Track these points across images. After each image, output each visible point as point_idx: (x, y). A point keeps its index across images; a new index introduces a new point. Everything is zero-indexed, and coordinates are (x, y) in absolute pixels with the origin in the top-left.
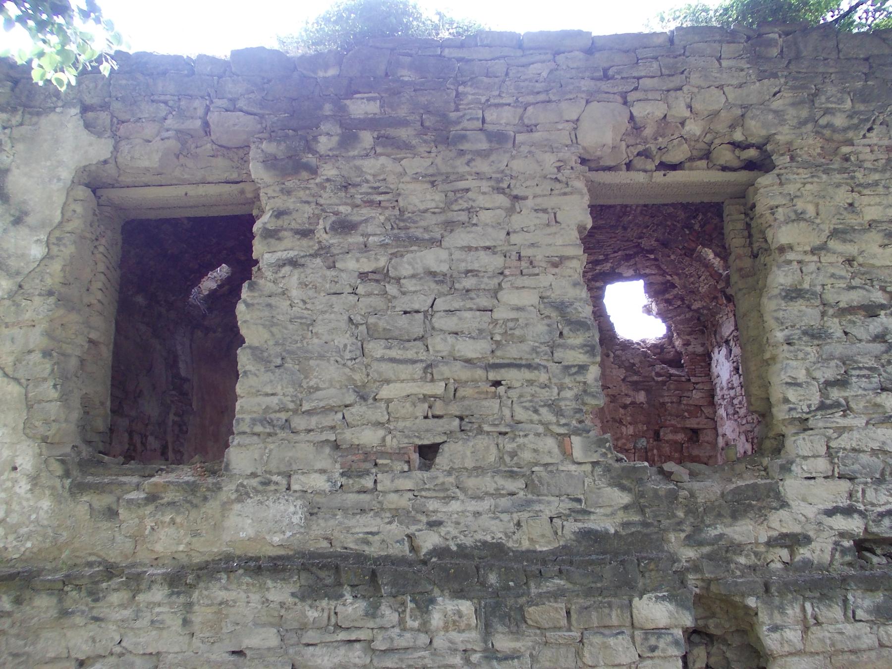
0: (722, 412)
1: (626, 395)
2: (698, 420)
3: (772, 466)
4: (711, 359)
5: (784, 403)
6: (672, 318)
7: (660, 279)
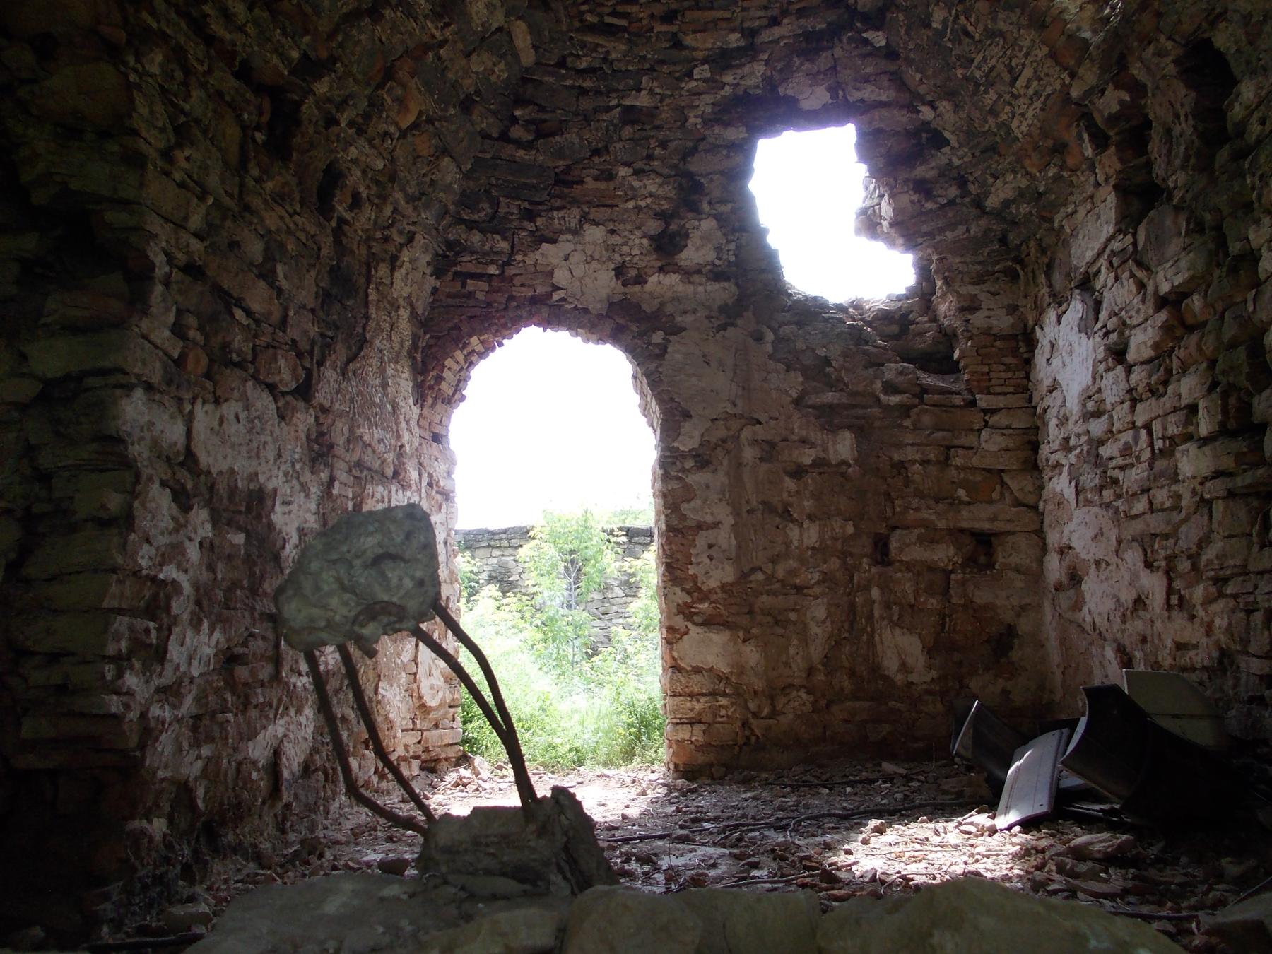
0: (1061, 485)
1: (803, 441)
2: (991, 509)
4: (1032, 344)
6: (931, 235)
7: (901, 118)
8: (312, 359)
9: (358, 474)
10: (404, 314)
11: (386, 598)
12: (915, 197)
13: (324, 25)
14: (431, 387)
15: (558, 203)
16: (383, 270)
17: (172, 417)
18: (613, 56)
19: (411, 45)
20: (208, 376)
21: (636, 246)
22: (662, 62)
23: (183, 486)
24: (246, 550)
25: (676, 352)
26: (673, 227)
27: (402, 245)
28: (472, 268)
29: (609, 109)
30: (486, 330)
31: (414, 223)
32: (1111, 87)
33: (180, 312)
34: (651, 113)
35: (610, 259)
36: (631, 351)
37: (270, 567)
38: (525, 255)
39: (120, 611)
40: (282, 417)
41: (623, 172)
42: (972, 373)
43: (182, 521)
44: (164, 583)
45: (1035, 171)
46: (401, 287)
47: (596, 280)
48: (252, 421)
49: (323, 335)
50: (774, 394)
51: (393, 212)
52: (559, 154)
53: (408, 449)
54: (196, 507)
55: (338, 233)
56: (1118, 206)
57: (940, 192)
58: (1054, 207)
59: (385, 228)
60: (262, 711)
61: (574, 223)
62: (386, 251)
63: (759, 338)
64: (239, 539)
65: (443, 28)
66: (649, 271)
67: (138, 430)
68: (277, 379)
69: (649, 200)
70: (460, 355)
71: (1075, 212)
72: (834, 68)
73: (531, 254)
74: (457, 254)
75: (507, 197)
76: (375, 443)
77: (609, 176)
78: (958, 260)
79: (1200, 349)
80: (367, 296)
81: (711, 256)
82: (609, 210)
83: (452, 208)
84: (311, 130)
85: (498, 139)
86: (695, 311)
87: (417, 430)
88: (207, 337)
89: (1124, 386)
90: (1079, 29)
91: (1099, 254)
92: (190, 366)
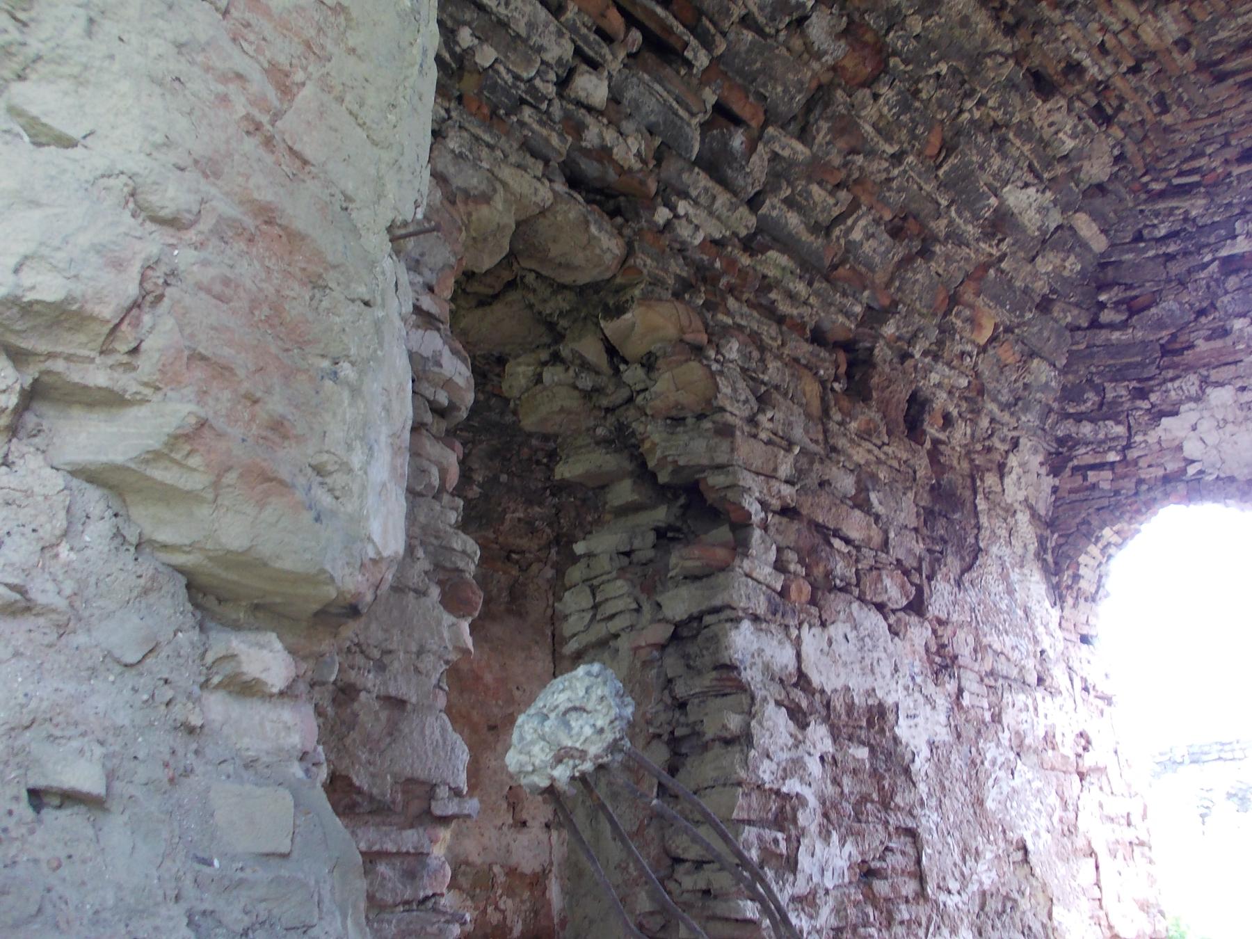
8: (921, 575)
9: (992, 683)
10: (1023, 518)
11: (570, 744)
13: (880, 277)
14: (1069, 587)
15: (1171, 373)
16: (991, 479)
17: (780, 642)
19: (970, 269)
20: (813, 601)
23: (799, 706)
24: (871, 764)
27: (1007, 452)
28: (1090, 459)
29: (1205, 266)
30: (1119, 519)
31: (1015, 428)
33: (779, 550)
37: (901, 780)
38: (1145, 434)
39: (750, 822)
40: (894, 632)
43: (800, 737)
44: (787, 797)
46: (1013, 491)
47: (1236, 443)
48: (863, 639)
51: (991, 423)
52: (1160, 324)
53: (1050, 653)
54: (813, 723)
55: (934, 456)
59: (984, 439)
60: (909, 927)
61: (1193, 390)
62: (991, 461)
64: (863, 753)
65: (997, 245)
67: (749, 657)
70: (1094, 550)
73: (1152, 433)
74: (1071, 449)
75: (1111, 381)
76: (1007, 650)
77: (1225, 333)
80: (976, 507)
82: (1233, 367)
83: (1055, 406)
84: (887, 370)
87: (1059, 634)
88: (807, 567)
92: (794, 595)
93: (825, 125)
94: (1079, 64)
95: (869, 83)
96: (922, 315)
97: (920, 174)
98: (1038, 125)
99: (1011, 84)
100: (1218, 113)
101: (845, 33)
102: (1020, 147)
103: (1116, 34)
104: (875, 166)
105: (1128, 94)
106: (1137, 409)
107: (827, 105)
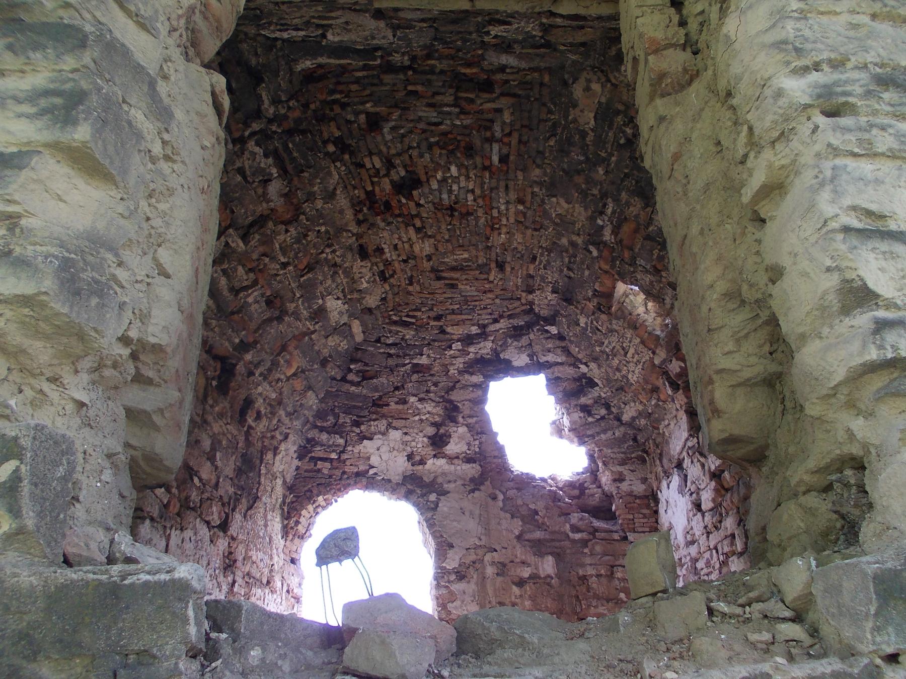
3: (834, 590)
4: (657, 501)
5: (846, 311)
6: (593, 436)
7: (570, 371)
10: (279, 482)
12: (582, 415)
13: (253, 325)
14: (292, 528)
15: (374, 417)
16: (269, 456)
18: (407, 337)
20: (178, 514)
21: (420, 443)
22: (434, 341)
25: (444, 507)
26: (442, 431)
27: (281, 441)
29: (405, 365)
31: (289, 428)
32: (674, 360)
34: (429, 368)
35: (404, 450)
36: (416, 505)
40: (212, 541)
41: (412, 399)
42: (623, 520)
45: (645, 401)
48: (197, 542)
49: (235, 493)
50: (504, 532)
52: (376, 389)
53: (276, 567)
55: (248, 434)
56: (689, 422)
57: (596, 412)
58: (659, 420)
61: (383, 428)
62: (271, 444)
63: (494, 498)
66: (428, 457)
68: (211, 518)
69: (427, 416)
70: (311, 508)
71: (669, 424)
72: (530, 344)
73: (357, 447)
74: (313, 446)
75: (343, 413)
77: (404, 402)
78: (610, 451)
79: (732, 502)
80: (260, 470)
81: (465, 448)
83: (311, 419)
84: (240, 379)
85: (341, 380)
86: (455, 481)
87: (282, 555)
88: (179, 492)
89: (702, 525)
90: (654, 330)
91: (683, 448)
92: (171, 508)
93: (257, 237)
94: (383, 249)
95: (287, 223)
96: (266, 352)
97: (292, 277)
98: (354, 270)
99: (350, 248)
100: (433, 293)
101: (286, 195)
102: (342, 279)
103: (403, 242)
104: (273, 266)
105: (398, 271)
106: (353, 432)
107: (262, 227)
